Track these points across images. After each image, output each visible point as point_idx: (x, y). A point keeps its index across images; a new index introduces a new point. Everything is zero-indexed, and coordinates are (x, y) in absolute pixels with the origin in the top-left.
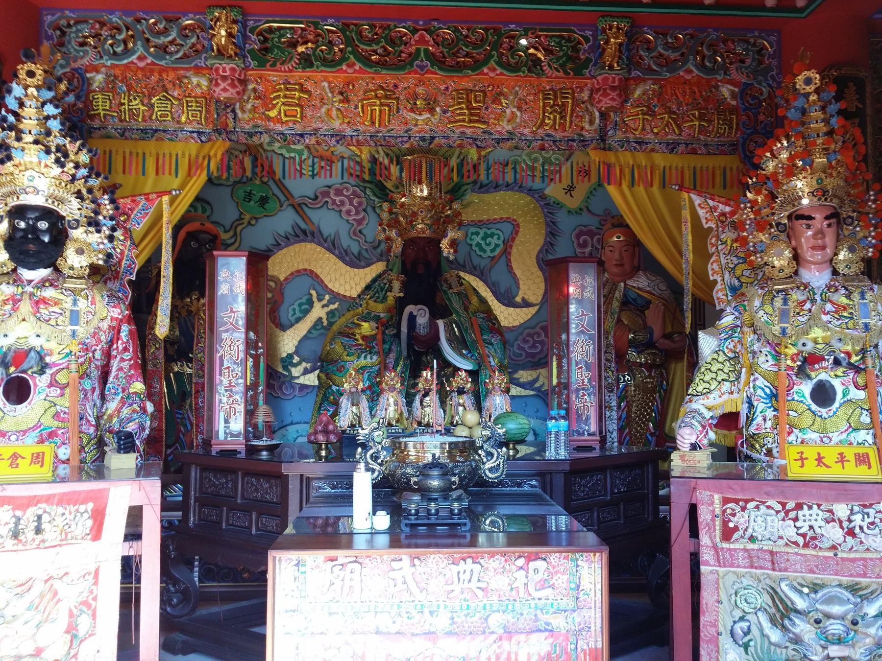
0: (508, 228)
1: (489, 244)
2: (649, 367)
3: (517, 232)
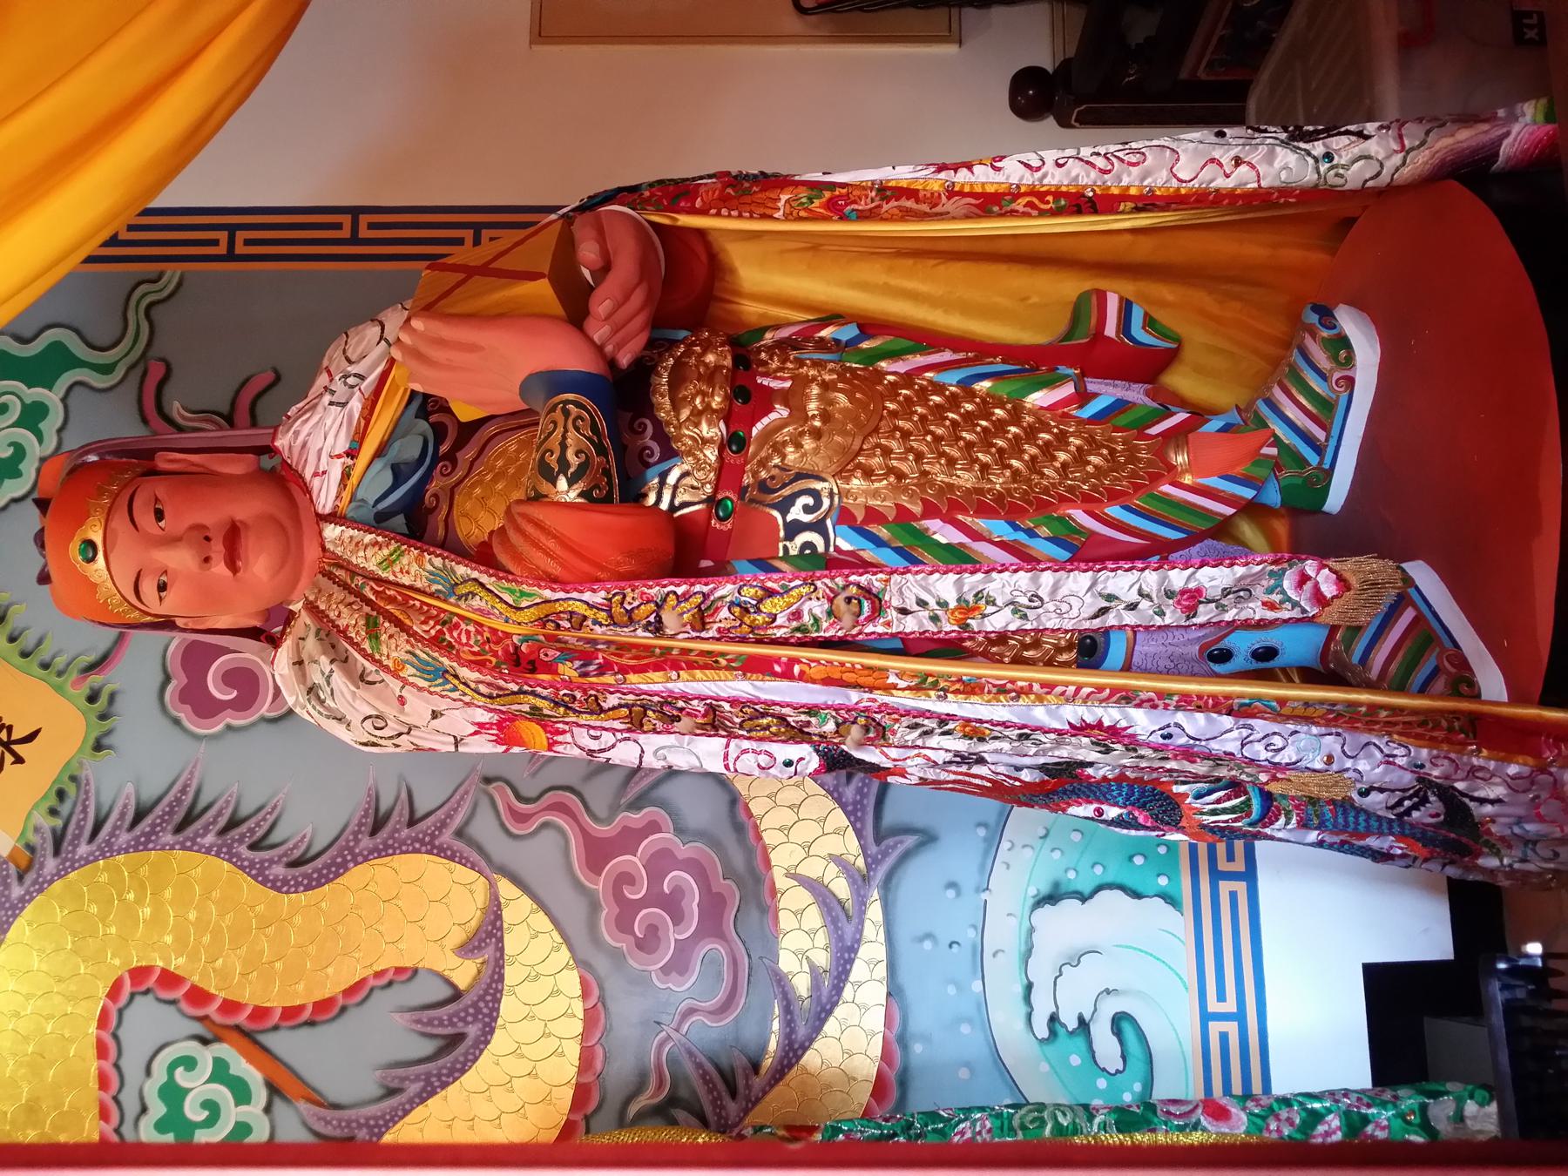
1: (212, 1107)
2: (746, 399)
3: (169, 979)
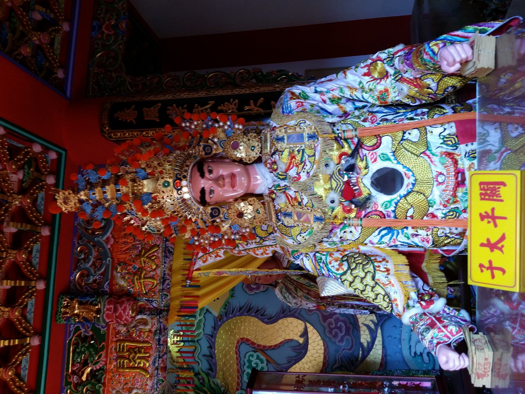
0: (244, 348)
3: (248, 340)
